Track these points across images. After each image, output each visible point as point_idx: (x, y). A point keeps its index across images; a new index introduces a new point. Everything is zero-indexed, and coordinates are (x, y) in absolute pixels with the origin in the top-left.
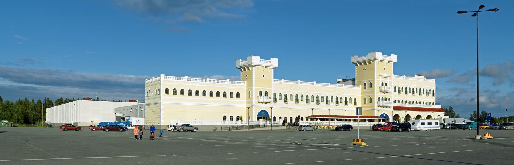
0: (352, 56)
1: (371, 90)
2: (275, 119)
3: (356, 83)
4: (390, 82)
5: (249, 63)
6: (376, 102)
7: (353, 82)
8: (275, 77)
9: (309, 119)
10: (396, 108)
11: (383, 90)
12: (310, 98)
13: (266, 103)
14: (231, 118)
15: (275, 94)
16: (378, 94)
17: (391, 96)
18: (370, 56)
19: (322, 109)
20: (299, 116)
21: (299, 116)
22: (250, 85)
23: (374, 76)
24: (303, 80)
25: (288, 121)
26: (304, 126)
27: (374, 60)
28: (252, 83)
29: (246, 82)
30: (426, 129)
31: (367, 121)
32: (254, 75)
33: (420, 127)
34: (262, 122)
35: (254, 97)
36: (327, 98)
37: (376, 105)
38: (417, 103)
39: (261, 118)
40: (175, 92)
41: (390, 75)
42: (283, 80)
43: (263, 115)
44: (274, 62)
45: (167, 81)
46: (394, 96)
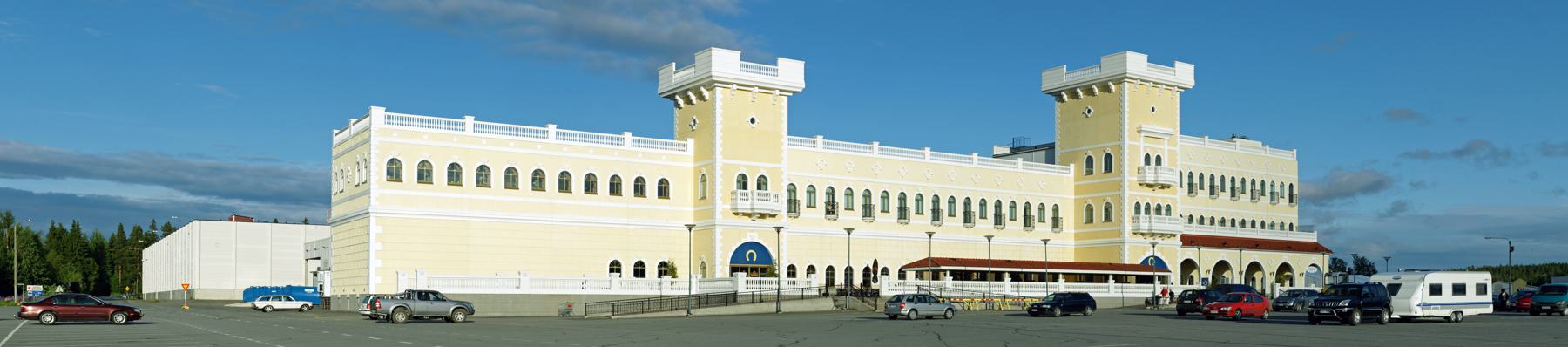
0: (1046, 68)
1: (1109, 178)
2: (792, 271)
3: (1057, 158)
4: (1172, 154)
5: (701, 74)
6: (1127, 219)
7: (1049, 153)
8: (792, 131)
9: (911, 274)
10: (1188, 241)
11: (1150, 178)
12: (975, 208)
13: (762, 216)
14: (640, 270)
15: (792, 189)
16: (1133, 194)
17: (1174, 200)
18: (1107, 67)
19: (957, 241)
20: (876, 264)
21: (876, 264)
22: (706, 152)
23: (1121, 130)
24: (938, 147)
25: (839, 279)
26: (911, 299)
27: (1120, 81)
28: (714, 145)
29: (691, 142)
30: (1447, 312)
31: (1111, 281)
32: (719, 119)
33: (1425, 306)
34: (743, 284)
35: (719, 195)
36: (968, 202)
37: (1128, 227)
38: (1243, 223)
39: (744, 269)
40: (511, 178)
41: (1170, 131)
42: (975, 155)
43: (753, 260)
44: (791, 73)
45: (387, 132)
46: (1178, 199)
